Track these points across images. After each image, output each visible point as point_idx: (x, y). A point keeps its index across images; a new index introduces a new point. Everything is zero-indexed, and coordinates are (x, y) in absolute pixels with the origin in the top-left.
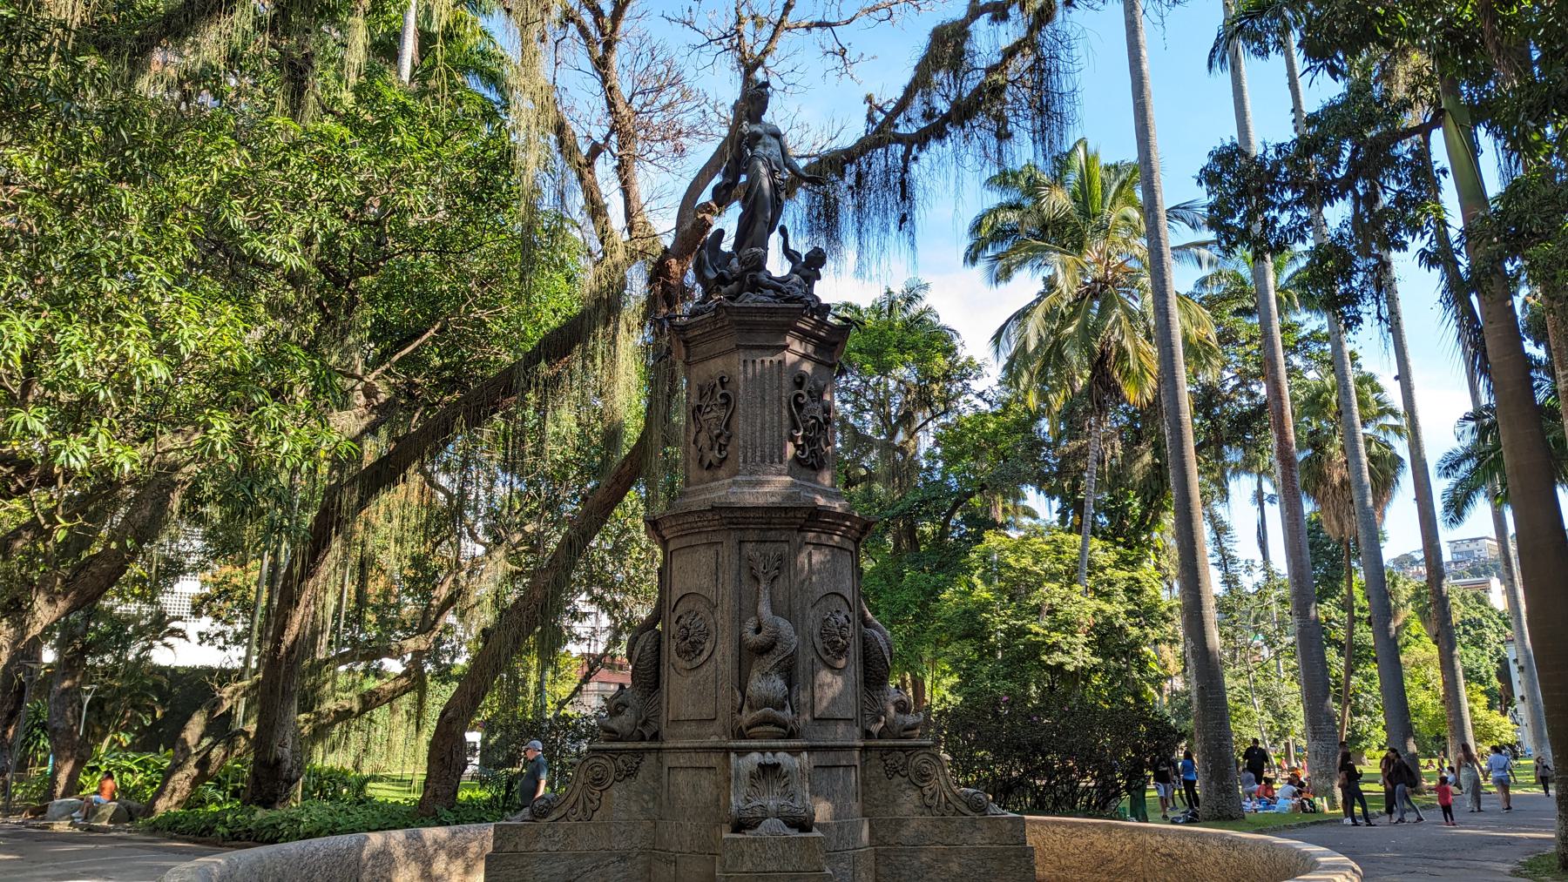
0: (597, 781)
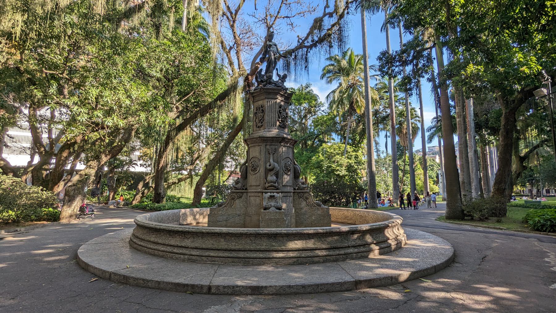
0: (233, 199)
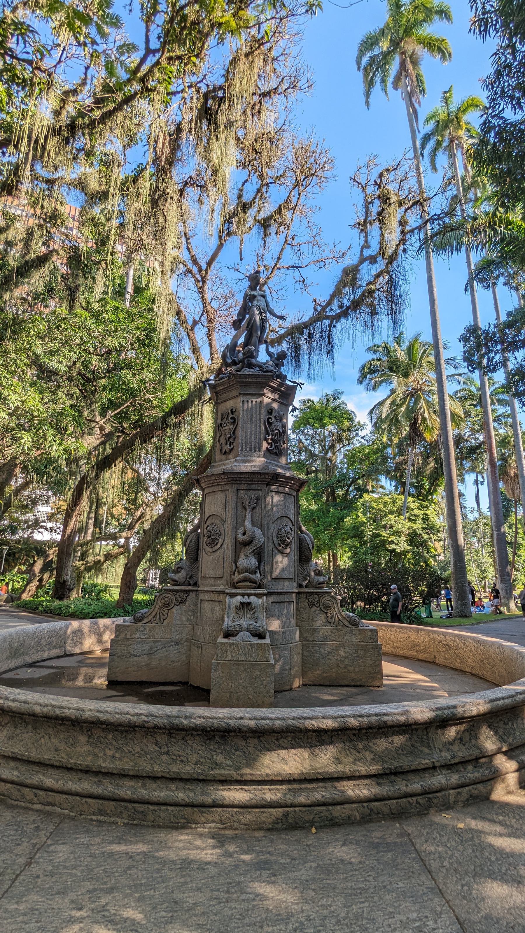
0: (167, 605)
